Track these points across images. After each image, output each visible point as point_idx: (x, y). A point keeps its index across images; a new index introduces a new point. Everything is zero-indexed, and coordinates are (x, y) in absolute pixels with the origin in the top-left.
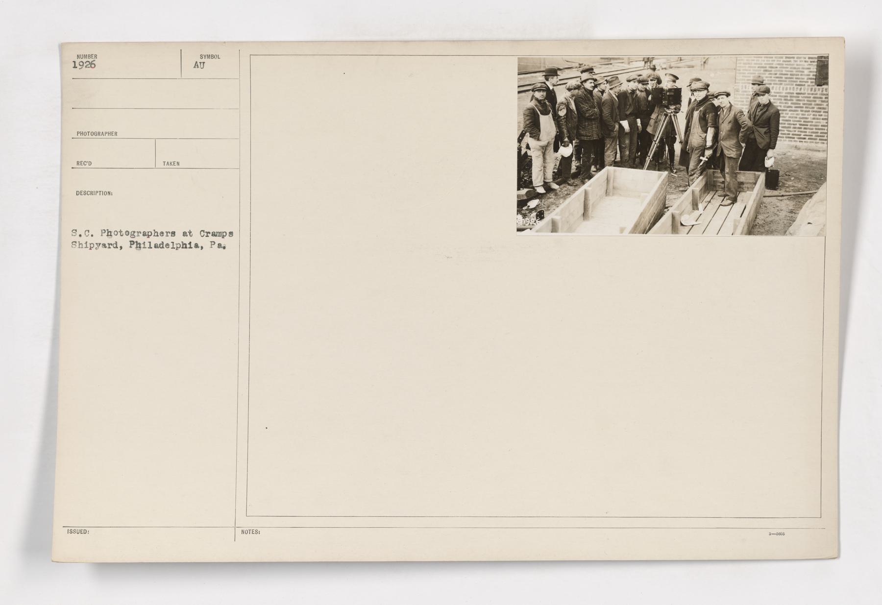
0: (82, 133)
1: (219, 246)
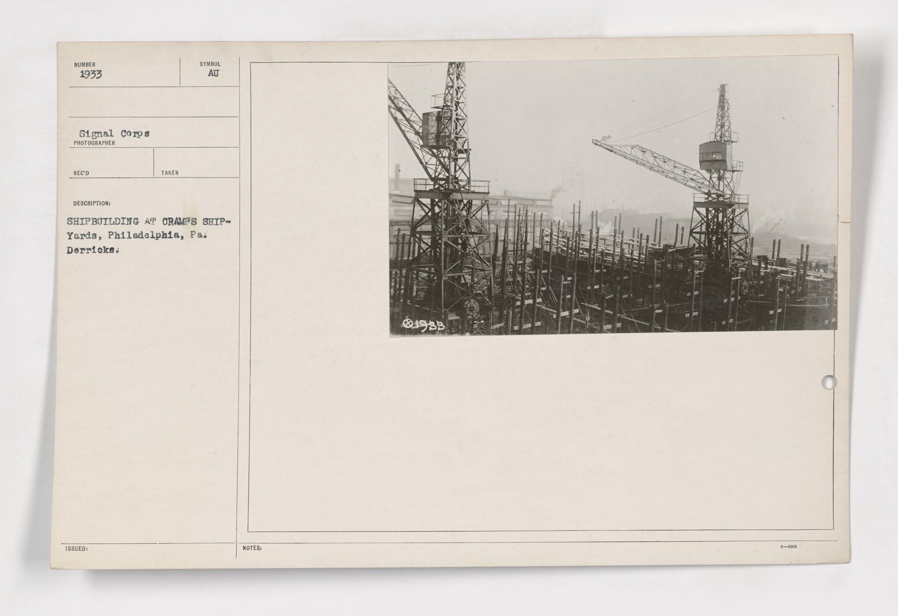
1: (200, 236)
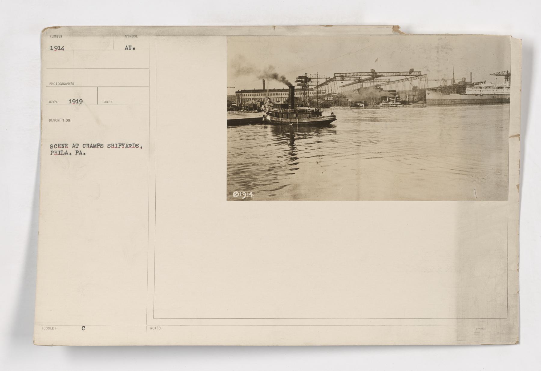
0: (52, 84)
